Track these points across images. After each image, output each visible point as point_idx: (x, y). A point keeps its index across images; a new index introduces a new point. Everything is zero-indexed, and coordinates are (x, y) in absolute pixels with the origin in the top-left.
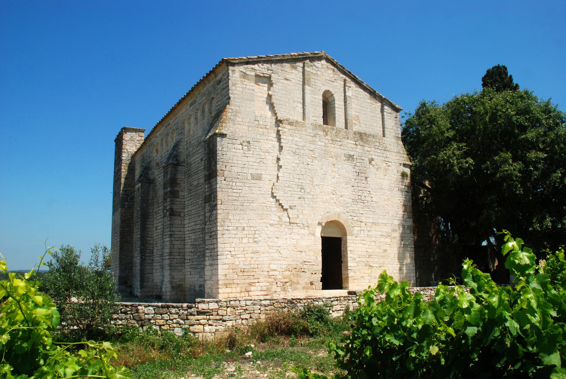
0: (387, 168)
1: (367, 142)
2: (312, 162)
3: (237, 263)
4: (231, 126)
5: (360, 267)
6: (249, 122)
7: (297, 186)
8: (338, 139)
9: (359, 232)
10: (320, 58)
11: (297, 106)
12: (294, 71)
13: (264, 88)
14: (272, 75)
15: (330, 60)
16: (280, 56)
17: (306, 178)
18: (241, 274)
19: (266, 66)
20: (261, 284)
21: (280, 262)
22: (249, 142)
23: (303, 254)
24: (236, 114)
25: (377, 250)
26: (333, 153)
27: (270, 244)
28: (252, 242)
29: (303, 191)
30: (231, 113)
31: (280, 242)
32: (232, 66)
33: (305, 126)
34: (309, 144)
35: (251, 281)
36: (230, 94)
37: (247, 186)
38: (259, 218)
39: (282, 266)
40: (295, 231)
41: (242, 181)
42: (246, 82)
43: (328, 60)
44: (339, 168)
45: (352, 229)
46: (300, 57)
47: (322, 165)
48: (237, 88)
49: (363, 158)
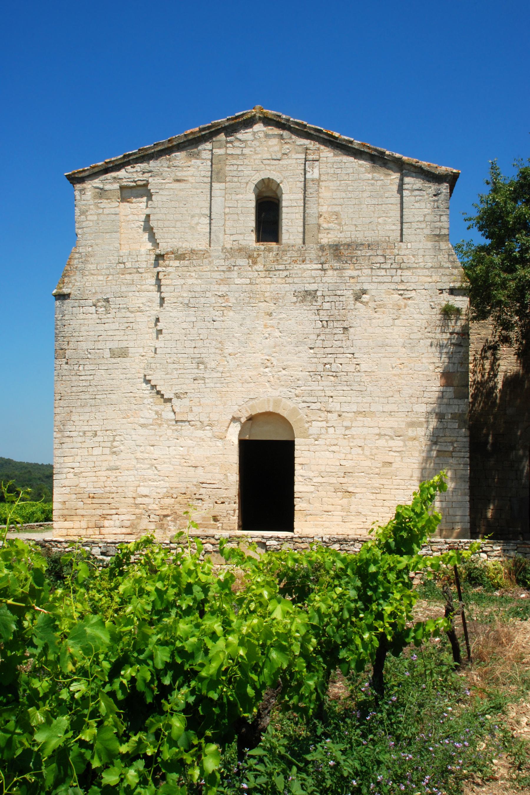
0: (402, 303)
1: (352, 259)
2: (223, 315)
3: (83, 485)
4: (78, 279)
5: (323, 494)
6: (107, 268)
7: (190, 360)
8: (281, 267)
9: (323, 431)
10: (249, 123)
11: (198, 224)
12: (194, 161)
13: (141, 205)
14: (150, 180)
15: (271, 120)
16: (163, 143)
17: (208, 345)
18: (89, 501)
19: (139, 167)
20: (122, 517)
21: (155, 483)
22: (107, 300)
23: (200, 471)
24: (86, 258)
25: (368, 463)
26: (267, 294)
27: (139, 455)
28: (108, 452)
29: (202, 366)
30: (79, 258)
31: (157, 453)
32: (79, 183)
33: (210, 256)
34: (217, 286)
35: (105, 512)
36: (77, 230)
37: (103, 368)
38: (122, 416)
39: (159, 490)
40: (184, 433)
41: (95, 361)
42: (105, 203)
43: (267, 121)
44: (280, 319)
45: (307, 425)
46: (203, 133)
47: (244, 319)
48: (89, 218)
49: (339, 293)
